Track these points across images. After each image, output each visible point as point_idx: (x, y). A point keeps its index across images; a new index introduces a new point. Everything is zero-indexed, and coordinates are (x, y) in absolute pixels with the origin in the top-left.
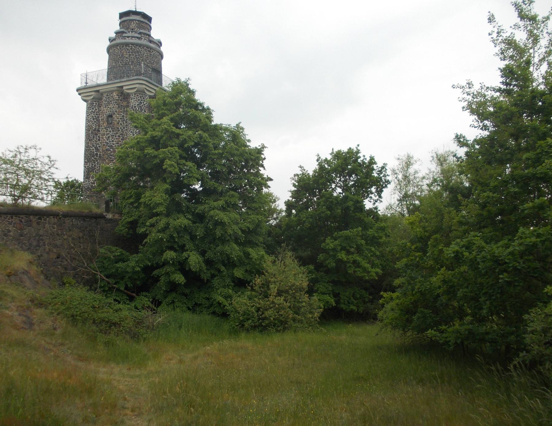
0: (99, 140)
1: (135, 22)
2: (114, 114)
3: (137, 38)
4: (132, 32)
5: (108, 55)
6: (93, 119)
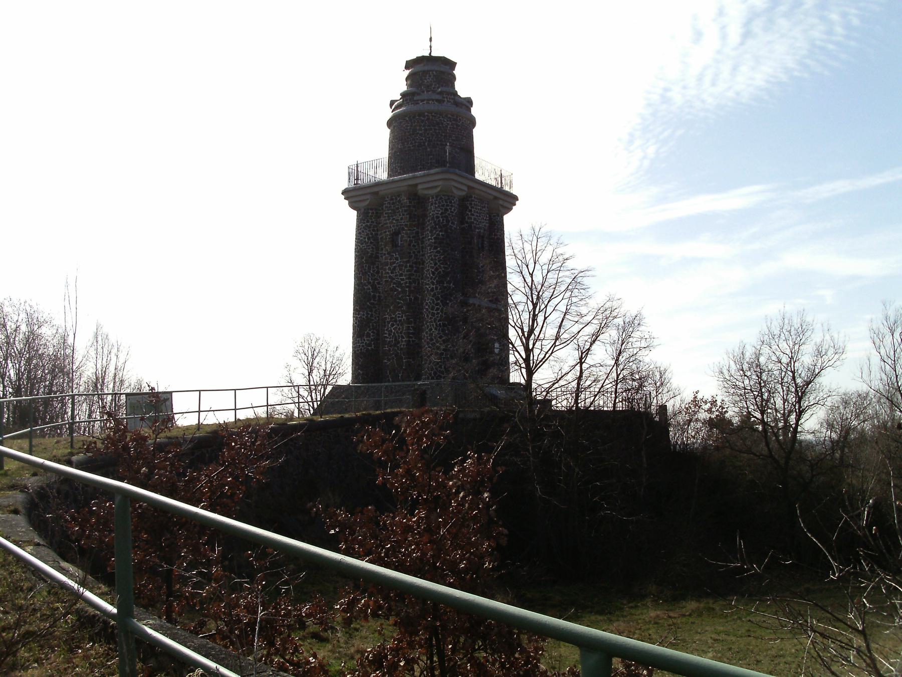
0: (378, 272)
1: (431, 76)
2: (403, 229)
3: (437, 101)
4: (428, 91)
5: (389, 131)
6: (369, 239)
